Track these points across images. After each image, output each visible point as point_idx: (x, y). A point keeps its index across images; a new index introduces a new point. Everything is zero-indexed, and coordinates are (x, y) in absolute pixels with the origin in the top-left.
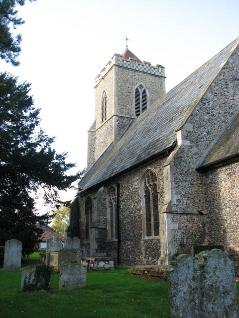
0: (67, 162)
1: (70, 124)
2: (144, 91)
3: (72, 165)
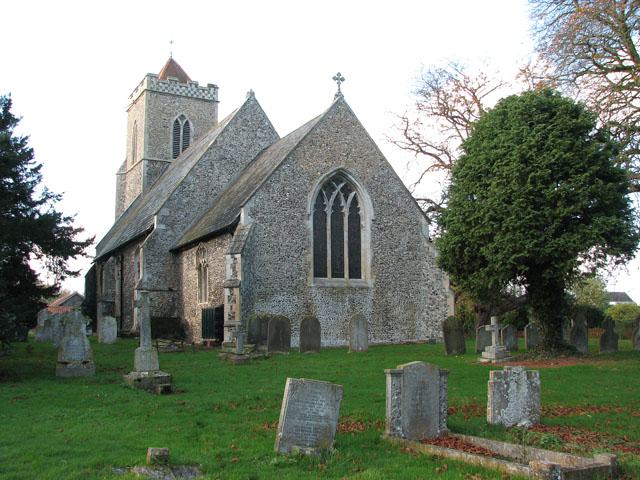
0: (75, 226)
1: (84, 180)
2: (187, 122)
3: (80, 230)
